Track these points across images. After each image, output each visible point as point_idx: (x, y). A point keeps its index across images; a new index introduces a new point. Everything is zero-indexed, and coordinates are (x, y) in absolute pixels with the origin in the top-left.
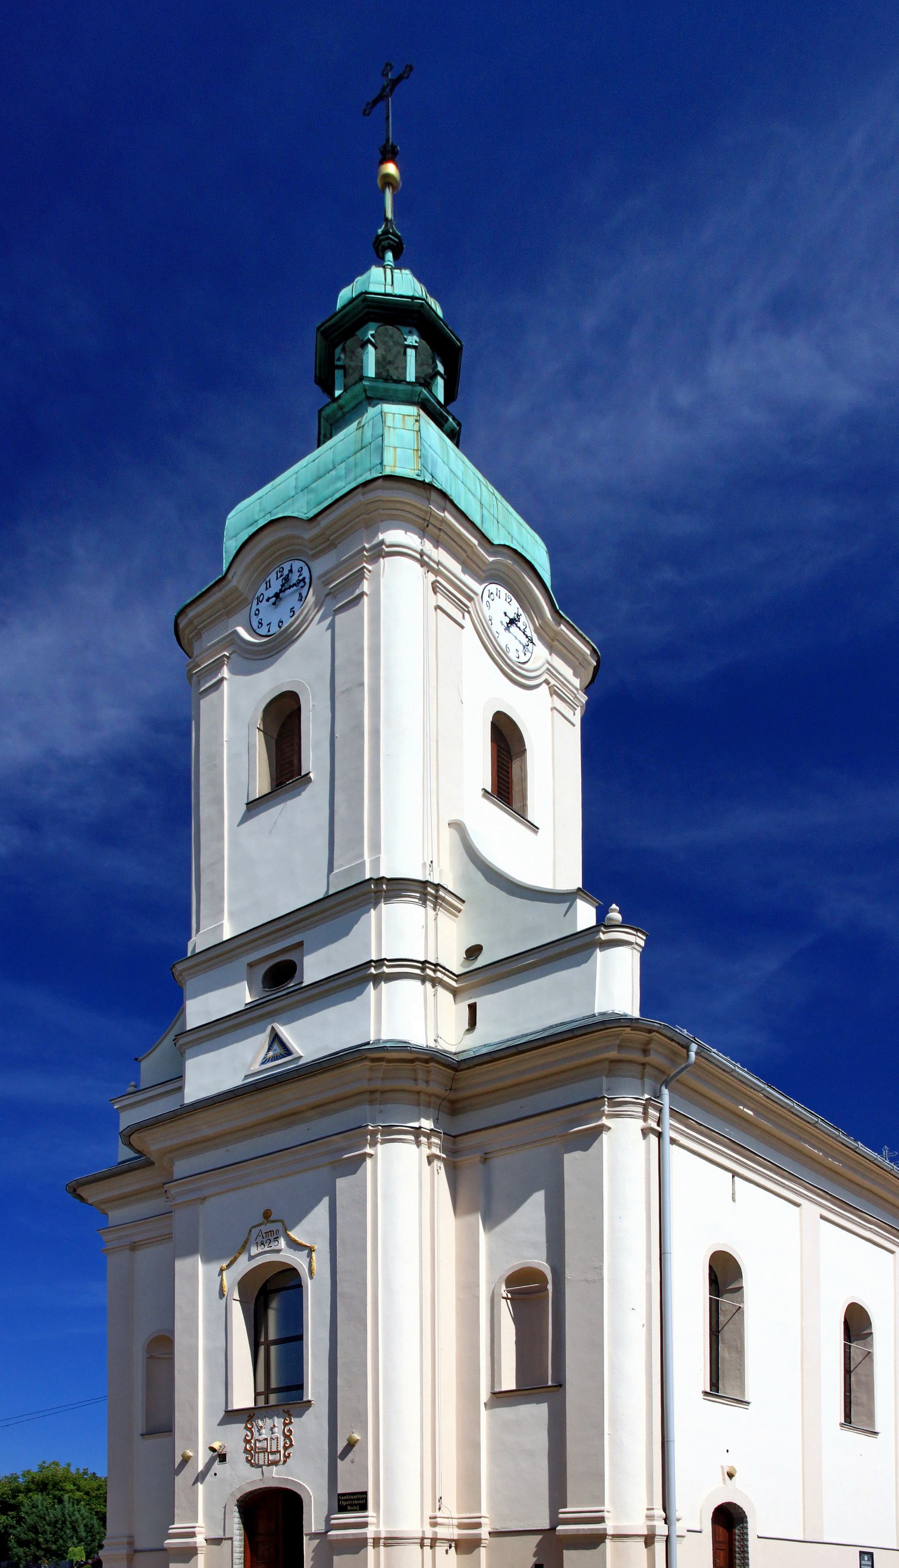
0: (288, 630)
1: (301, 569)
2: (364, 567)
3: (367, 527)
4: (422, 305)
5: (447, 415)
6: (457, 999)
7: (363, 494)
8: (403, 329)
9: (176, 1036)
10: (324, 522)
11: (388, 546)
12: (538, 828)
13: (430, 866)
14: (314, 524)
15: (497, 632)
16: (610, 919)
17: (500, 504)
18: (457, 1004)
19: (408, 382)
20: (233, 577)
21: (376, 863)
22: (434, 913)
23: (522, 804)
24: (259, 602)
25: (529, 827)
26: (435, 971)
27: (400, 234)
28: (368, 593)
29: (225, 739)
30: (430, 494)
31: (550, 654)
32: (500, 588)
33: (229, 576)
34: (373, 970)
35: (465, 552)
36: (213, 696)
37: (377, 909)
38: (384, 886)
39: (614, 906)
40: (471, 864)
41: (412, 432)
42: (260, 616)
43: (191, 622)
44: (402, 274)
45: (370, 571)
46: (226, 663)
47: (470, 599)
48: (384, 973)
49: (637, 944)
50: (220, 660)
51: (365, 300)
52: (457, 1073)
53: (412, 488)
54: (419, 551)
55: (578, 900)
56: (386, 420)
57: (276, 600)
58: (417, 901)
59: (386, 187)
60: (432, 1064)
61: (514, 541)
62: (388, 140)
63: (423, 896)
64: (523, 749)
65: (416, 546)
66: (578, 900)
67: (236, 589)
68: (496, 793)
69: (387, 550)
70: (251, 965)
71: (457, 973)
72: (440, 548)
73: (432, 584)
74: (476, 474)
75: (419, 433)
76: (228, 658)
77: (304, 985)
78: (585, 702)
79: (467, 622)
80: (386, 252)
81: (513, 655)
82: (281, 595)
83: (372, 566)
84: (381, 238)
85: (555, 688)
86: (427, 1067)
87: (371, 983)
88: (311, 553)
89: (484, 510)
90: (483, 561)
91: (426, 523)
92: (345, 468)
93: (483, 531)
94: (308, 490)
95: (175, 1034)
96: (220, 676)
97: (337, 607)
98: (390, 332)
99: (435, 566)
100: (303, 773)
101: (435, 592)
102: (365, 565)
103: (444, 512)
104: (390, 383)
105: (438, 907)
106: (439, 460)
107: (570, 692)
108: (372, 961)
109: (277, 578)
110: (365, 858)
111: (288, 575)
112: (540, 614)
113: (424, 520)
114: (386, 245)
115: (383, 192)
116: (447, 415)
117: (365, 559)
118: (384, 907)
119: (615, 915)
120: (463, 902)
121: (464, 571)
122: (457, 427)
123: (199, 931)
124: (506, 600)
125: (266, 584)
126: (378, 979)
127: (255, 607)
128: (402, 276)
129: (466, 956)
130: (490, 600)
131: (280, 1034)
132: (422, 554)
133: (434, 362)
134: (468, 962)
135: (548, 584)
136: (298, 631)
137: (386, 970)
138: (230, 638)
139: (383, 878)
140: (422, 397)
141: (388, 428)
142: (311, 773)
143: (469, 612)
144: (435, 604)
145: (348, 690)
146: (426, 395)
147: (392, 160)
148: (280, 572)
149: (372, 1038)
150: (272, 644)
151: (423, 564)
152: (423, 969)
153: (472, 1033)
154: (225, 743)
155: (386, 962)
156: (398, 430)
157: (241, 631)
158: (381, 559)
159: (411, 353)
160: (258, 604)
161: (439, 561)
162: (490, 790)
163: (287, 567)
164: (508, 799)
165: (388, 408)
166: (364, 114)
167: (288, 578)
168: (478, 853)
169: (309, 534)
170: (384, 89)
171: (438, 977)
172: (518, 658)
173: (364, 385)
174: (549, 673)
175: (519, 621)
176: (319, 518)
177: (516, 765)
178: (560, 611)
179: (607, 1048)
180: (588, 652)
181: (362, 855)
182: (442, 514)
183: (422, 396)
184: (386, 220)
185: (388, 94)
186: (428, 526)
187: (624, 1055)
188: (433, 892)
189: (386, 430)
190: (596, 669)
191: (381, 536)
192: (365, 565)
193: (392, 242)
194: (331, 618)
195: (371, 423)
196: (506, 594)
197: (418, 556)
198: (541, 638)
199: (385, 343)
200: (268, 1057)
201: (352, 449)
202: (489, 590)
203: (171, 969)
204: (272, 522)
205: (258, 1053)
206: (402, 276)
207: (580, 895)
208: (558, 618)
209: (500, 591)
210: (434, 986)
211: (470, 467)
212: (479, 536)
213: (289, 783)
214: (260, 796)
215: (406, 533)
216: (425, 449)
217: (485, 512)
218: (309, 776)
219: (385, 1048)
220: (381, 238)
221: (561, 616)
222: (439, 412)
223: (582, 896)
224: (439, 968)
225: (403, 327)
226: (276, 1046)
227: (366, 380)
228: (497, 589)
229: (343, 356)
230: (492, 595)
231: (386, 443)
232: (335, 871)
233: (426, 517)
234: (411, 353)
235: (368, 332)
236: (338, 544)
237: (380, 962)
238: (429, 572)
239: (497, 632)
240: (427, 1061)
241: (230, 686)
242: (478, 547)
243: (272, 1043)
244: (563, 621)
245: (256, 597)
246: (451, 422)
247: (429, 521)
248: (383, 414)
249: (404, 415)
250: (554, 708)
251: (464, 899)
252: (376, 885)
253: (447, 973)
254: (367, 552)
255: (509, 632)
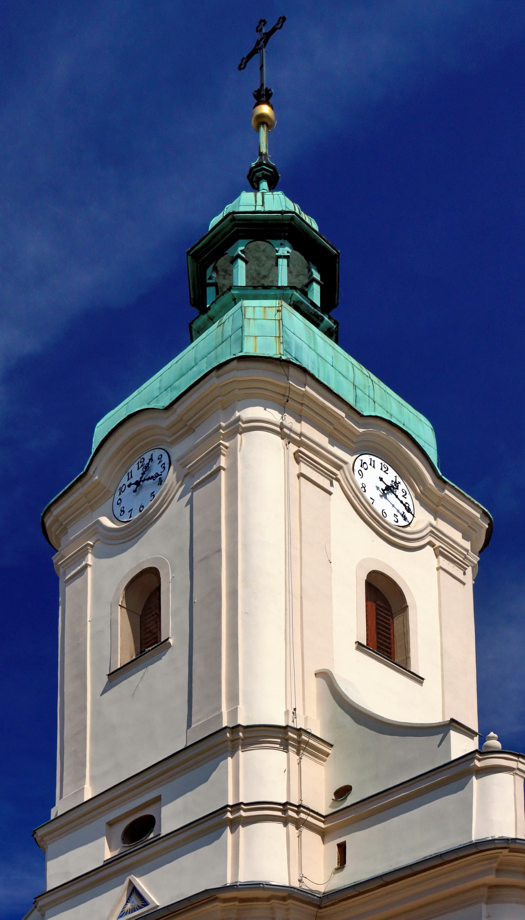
0: (148, 512)
1: (160, 456)
2: (221, 444)
3: (224, 409)
4: (292, 218)
5: (322, 315)
6: (326, 839)
7: (218, 377)
8: (273, 242)
9: (35, 898)
10: (180, 408)
11: (244, 423)
12: (423, 679)
13: (293, 713)
14: (170, 412)
15: (371, 498)
16: (487, 747)
17: (376, 386)
18: (326, 844)
19: (280, 287)
20: (94, 472)
21: (234, 713)
22: (298, 757)
23: (405, 657)
24: (121, 491)
25: (412, 678)
26: (298, 813)
27: (274, 165)
28: (225, 467)
29: (89, 619)
30: (289, 371)
31: (435, 519)
32: (374, 458)
33: (91, 472)
34: (229, 815)
35: (332, 424)
36: (77, 582)
37: (234, 757)
38: (241, 734)
39: (492, 734)
40: (339, 709)
41: (274, 320)
42: (122, 505)
43: (56, 520)
44: (273, 195)
45: (227, 448)
46: (90, 551)
47: (339, 468)
48: (241, 816)
49: (518, 769)
50: (85, 549)
51: (233, 219)
52: (320, 911)
53: (270, 366)
54: (279, 424)
55: (451, 731)
56: (246, 313)
57: (137, 488)
58: (278, 746)
59: (260, 126)
60: (290, 901)
61: (392, 417)
62: (262, 85)
63: (284, 741)
64: (404, 606)
65: (276, 420)
66: (452, 732)
67: (98, 483)
68: (376, 648)
69: (243, 426)
70: (110, 824)
71: (324, 814)
72: (303, 422)
73: (294, 454)
74: (349, 359)
75: (281, 321)
76: (92, 546)
77: (161, 836)
78: (476, 562)
79: (336, 489)
80: (261, 182)
81: (390, 519)
82: (141, 483)
83: (228, 442)
84: (254, 170)
85: (441, 549)
86: (286, 905)
87: (228, 827)
88: (170, 440)
89: (358, 391)
90: (353, 433)
91: (286, 398)
92: (207, 363)
93: (358, 409)
94: (171, 388)
95: (35, 897)
96: (84, 563)
97: (195, 483)
98: (262, 248)
99: (297, 438)
100: (162, 640)
101: (298, 462)
102: (221, 441)
103: (304, 387)
104: (259, 289)
105: (302, 751)
106: (305, 346)
107: (459, 553)
108: (228, 806)
109: (138, 468)
110: (223, 710)
111: (148, 464)
112: (422, 481)
113: (284, 396)
114: (261, 176)
115: (258, 131)
116: (322, 315)
117: (222, 437)
118: (241, 755)
119: (495, 743)
120: (332, 746)
121: (331, 443)
122: (334, 326)
123: (62, 798)
124: (381, 469)
125: (128, 475)
126: (234, 824)
127: (117, 497)
128: (273, 197)
129: (335, 797)
130: (363, 470)
131: (137, 886)
132: (282, 426)
133: (309, 270)
134: (336, 803)
135: (434, 458)
136: (158, 512)
137: (243, 814)
138: (94, 527)
139: (239, 726)
140: (294, 300)
141: (248, 320)
142: (170, 639)
143: (338, 480)
144: (298, 472)
145: (206, 558)
146: (298, 297)
147: (267, 102)
148: (141, 462)
149: (229, 881)
150: (134, 527)
151: (283, 436)
152: (284, 811)
153: (342, 871)
154: (89, 624)
155: (242, 806)
156: (258, 321)
157: (106, 521)
158: (239, 436)
159: (283, 263)
160: (120, 494)
161: (301, 432)
162: (365, 643)
163: (147, 457)
164: (390, 654)
165: (246, 303)
166: (240, 69)
167: (148, 466)
168: (346, 699)
169: (166, 421)
170: (258, 43)
171: (301, 818)
172: (397, 522)
173: (233, 294)
174: (433, 535)
175: (398, 489)
176: (175, 406)
177: (397, 622)
178: (443, 477)
179: (484, 873)
180: (478, 515)
181: (220, 708)
182: (303, 389)
183: (293, 299)
184: (261, 154)
185: (262, 46)
186: (288, 401)
187: (504, 880)
188: (295, 737)
189: (246, 321)
190: (489, 533)
191: (237, 414)
192: (221, 441)
193: (266, 173)
194: (190, 494)
195: (231, 318)
196: (382, 464)
197: (278, 429)
198: (423, 504)
199: (258, 259)
200: (126, 910)
201: (213, 344)
202: (362, 460)
203: (33, 836)
204: (130, 417)
205: (116, 907)
206: (273, 197)
207: (453, 726)
208: (441, 484)
209: (374, 461)
210: (297, 828)
211: (343, 354)
212: (346, 408)
213: (149, 651)
214: (122, 666)
215: (265, 409)
216: (288, 336)
217: (359, 392)
218: (168, 642)
219: (235, 887)
220: (254, 170)
221: (445, 482)
222: (313, 313)
223: (455, 727)
224: (302, 809)
225: (275, 241)
226: (134, 898)
227: (234, 290)
228: (371, 459)
229: (214, 275)
230: (365, 465)
231: (246, 333)
232: (193, 726)
233: (285, 392)
234: (283, 263)
235: (238, 249)
236: (195, 428)
237: (237, 806)
238: (290, 443)
239: (371, 498)
240: (284, 899)
241: (93, 572)
242: (345, 419)
243: (130, 896)
244: (447, 486)
245: (119, 488)
246: (327, 321)
247: (288, 397)
248: (243, 308)
249: (265, 307)
250: (439, 568)
251: (331, 743)
252: (232, 733)
253: (311, 813)
254: (223, 430)
255: (386, 498)
